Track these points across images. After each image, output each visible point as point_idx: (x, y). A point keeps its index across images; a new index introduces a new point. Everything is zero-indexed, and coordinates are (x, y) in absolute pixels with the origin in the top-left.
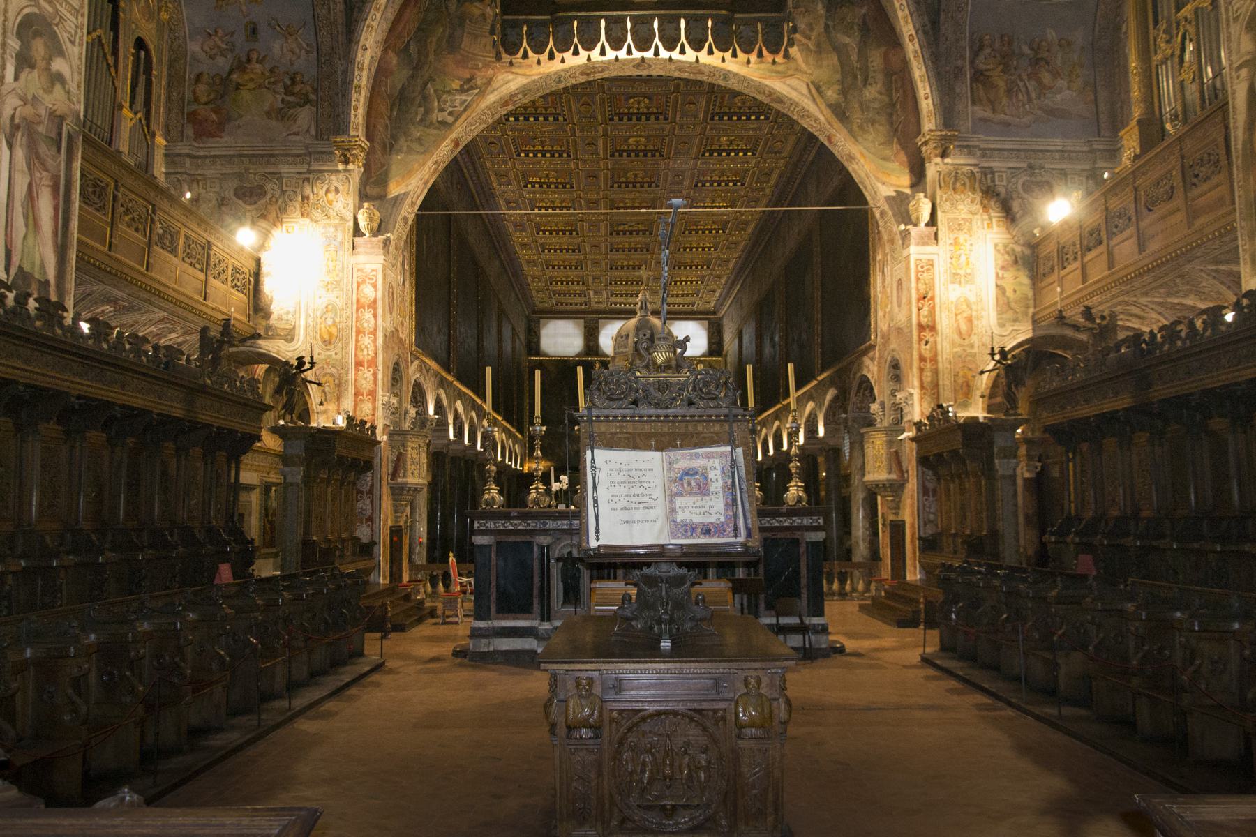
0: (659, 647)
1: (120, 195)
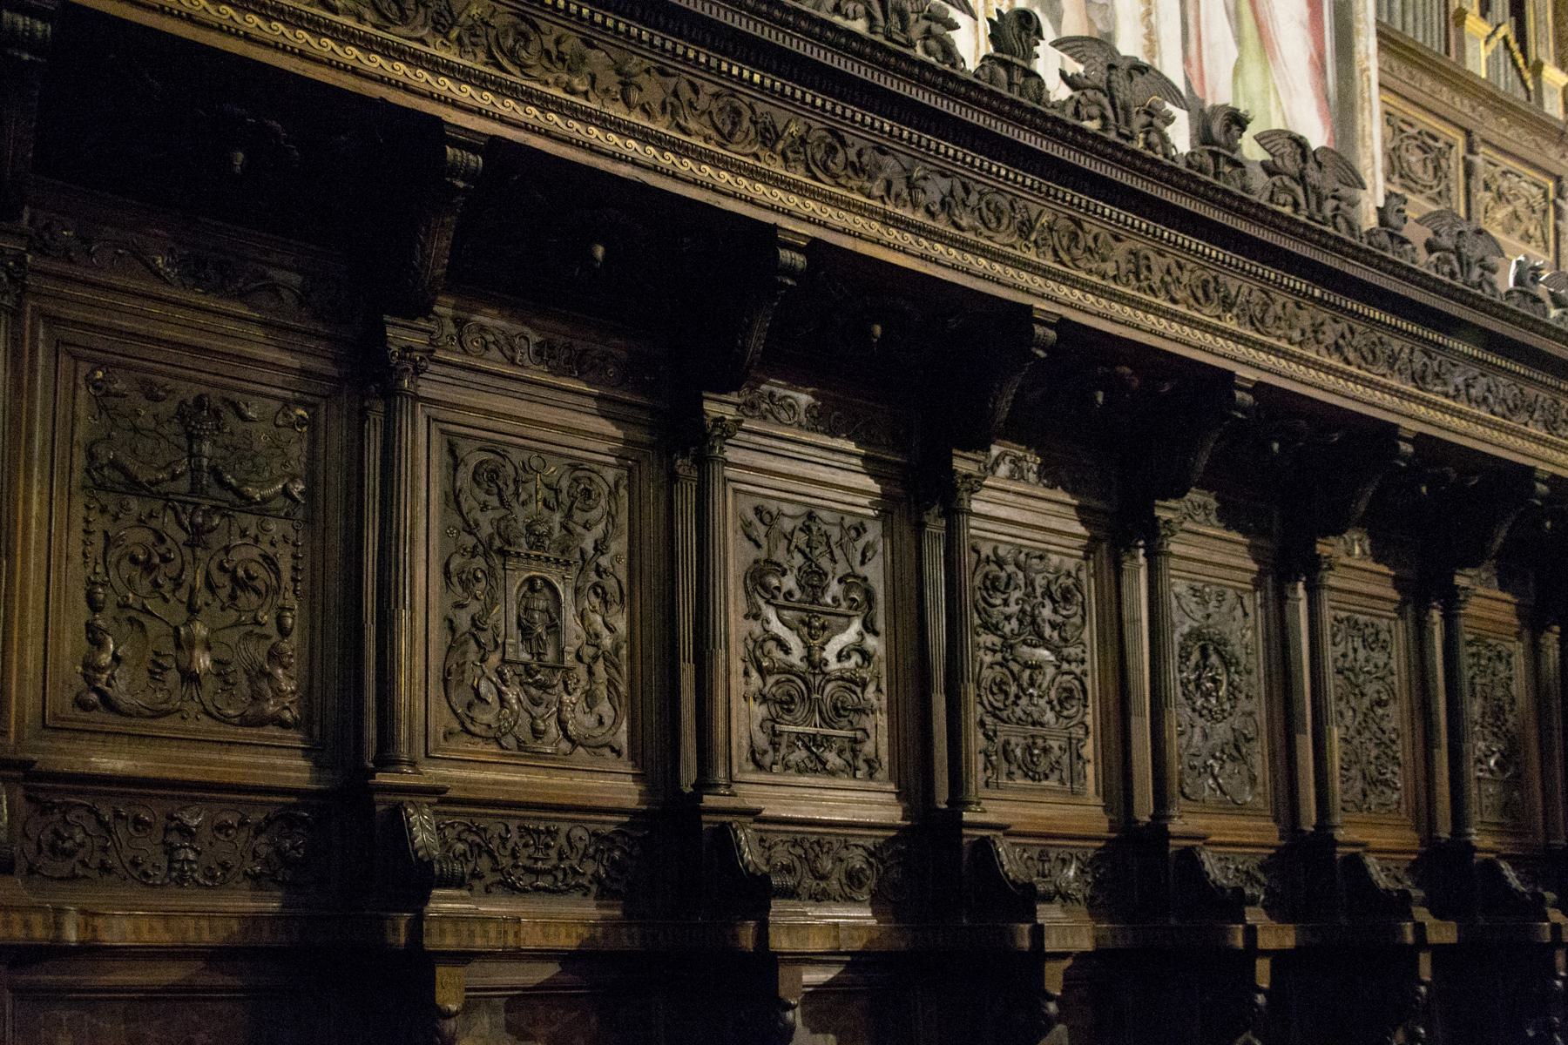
0: (600, 243)
1: (1478, 160)
